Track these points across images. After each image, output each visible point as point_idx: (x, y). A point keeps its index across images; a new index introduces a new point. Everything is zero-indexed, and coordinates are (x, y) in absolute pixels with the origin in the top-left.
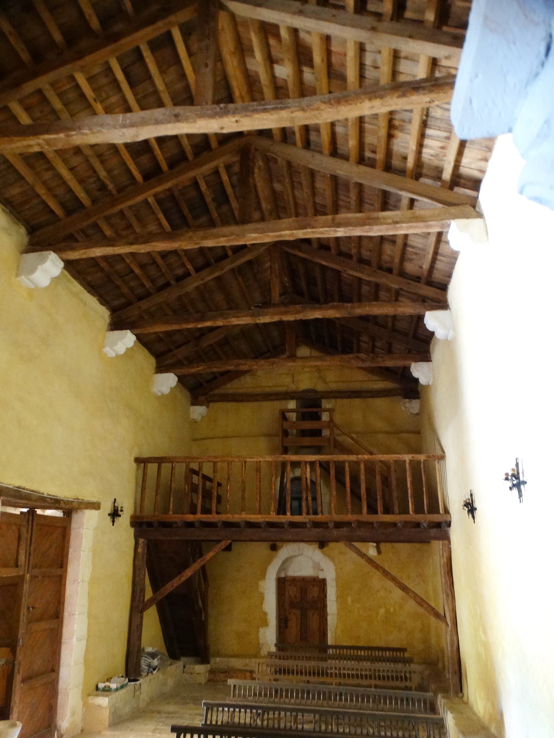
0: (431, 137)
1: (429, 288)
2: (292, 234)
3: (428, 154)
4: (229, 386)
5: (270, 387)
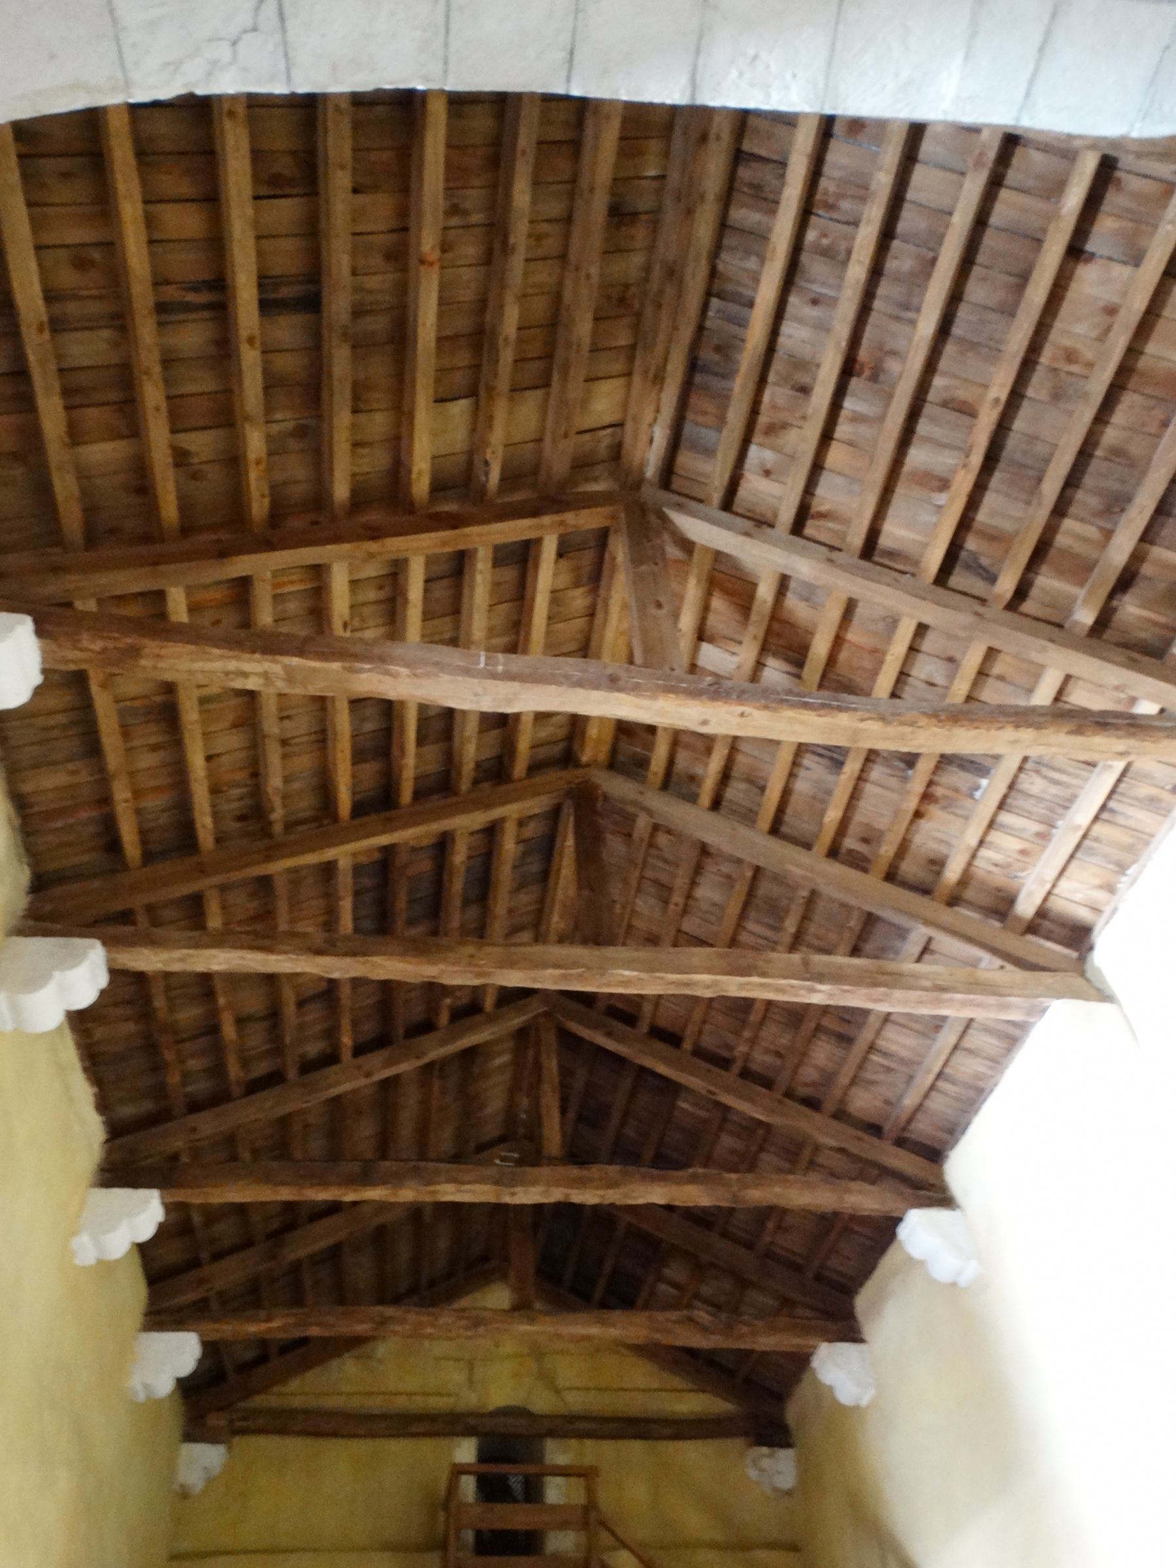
0: (1006, 829)
1: (901, 1152)
2: (715, 984)
3: (988, 860)
4: (294, 1384)
5: (410, 1394)
